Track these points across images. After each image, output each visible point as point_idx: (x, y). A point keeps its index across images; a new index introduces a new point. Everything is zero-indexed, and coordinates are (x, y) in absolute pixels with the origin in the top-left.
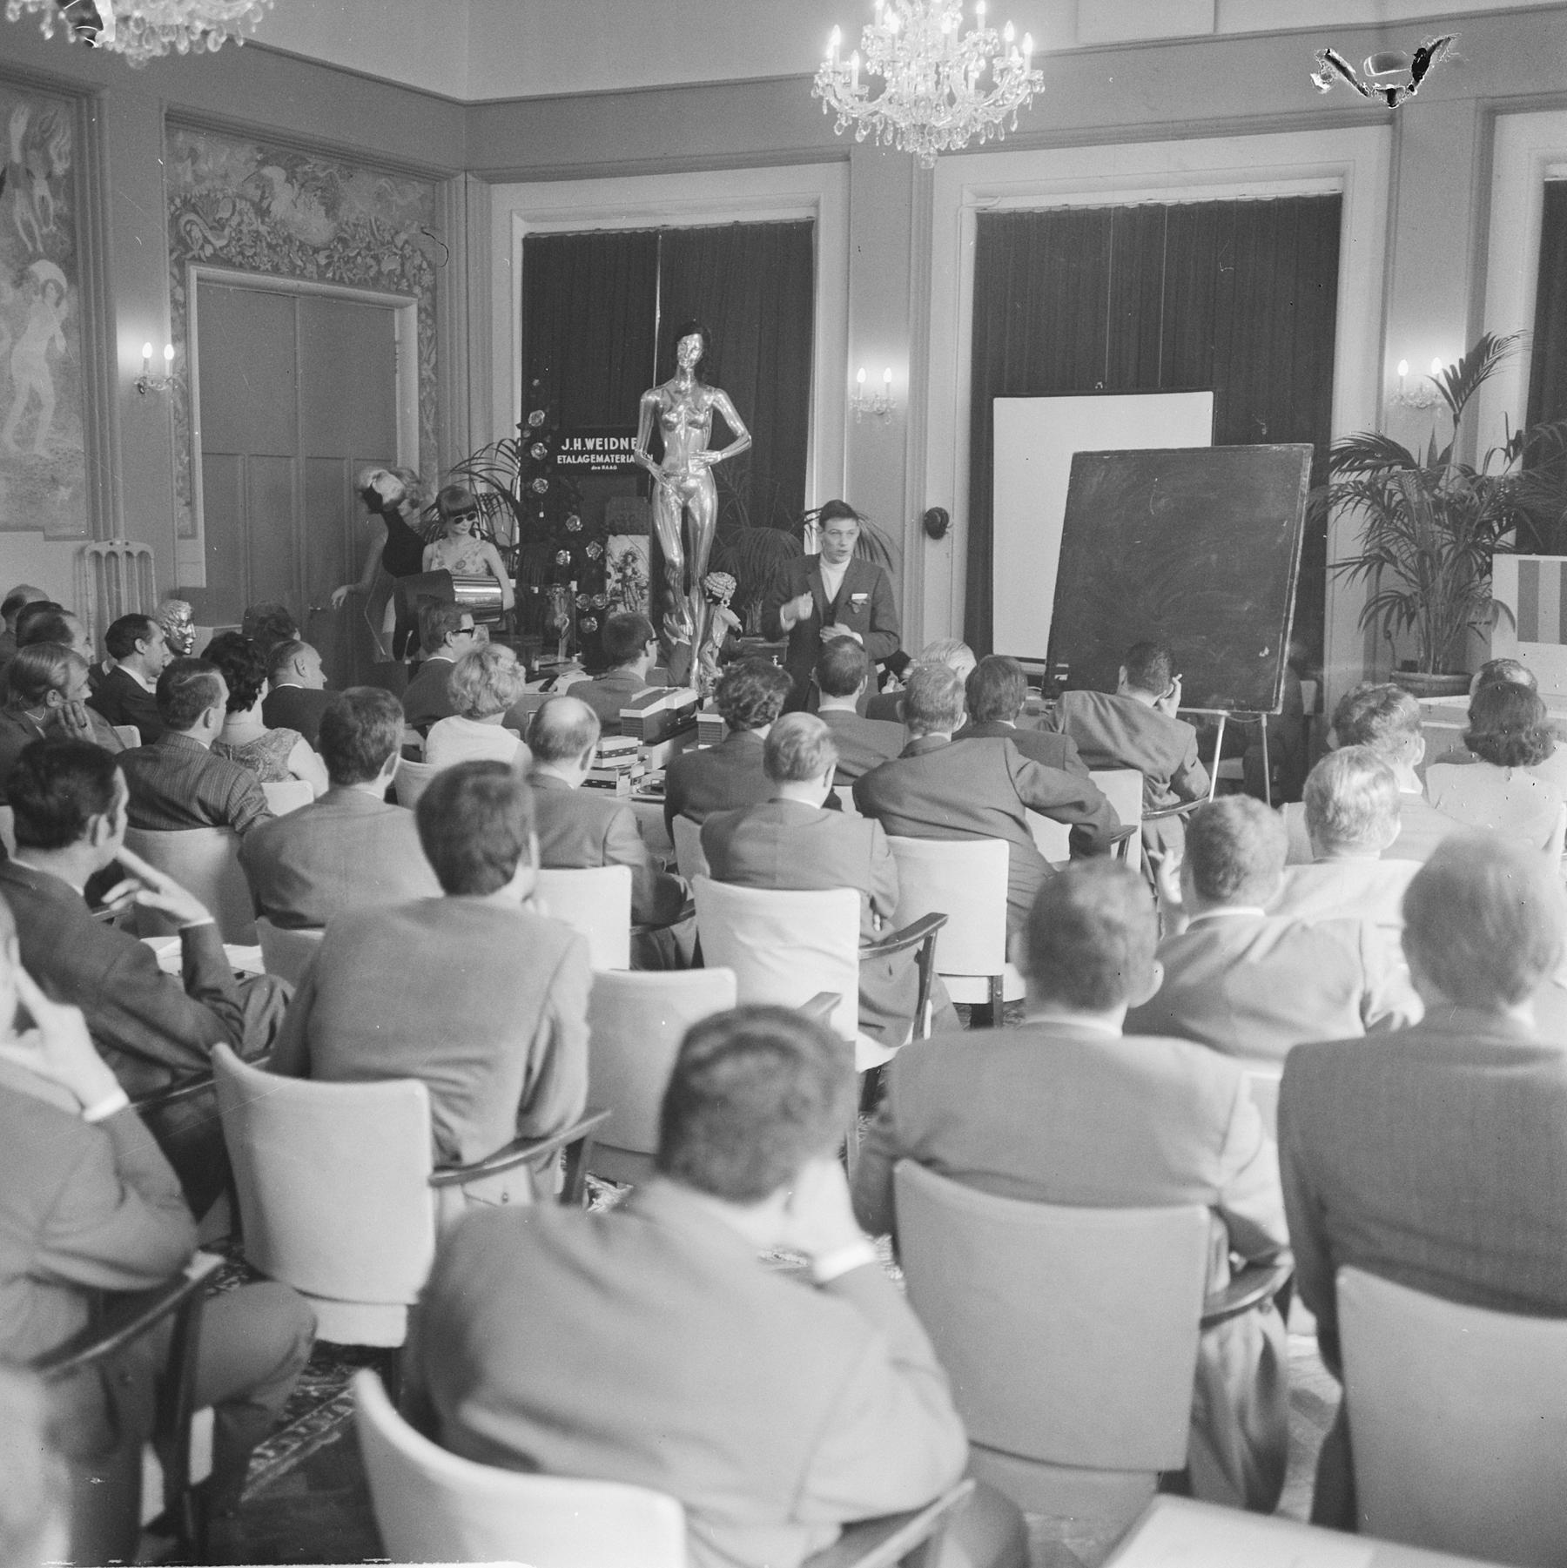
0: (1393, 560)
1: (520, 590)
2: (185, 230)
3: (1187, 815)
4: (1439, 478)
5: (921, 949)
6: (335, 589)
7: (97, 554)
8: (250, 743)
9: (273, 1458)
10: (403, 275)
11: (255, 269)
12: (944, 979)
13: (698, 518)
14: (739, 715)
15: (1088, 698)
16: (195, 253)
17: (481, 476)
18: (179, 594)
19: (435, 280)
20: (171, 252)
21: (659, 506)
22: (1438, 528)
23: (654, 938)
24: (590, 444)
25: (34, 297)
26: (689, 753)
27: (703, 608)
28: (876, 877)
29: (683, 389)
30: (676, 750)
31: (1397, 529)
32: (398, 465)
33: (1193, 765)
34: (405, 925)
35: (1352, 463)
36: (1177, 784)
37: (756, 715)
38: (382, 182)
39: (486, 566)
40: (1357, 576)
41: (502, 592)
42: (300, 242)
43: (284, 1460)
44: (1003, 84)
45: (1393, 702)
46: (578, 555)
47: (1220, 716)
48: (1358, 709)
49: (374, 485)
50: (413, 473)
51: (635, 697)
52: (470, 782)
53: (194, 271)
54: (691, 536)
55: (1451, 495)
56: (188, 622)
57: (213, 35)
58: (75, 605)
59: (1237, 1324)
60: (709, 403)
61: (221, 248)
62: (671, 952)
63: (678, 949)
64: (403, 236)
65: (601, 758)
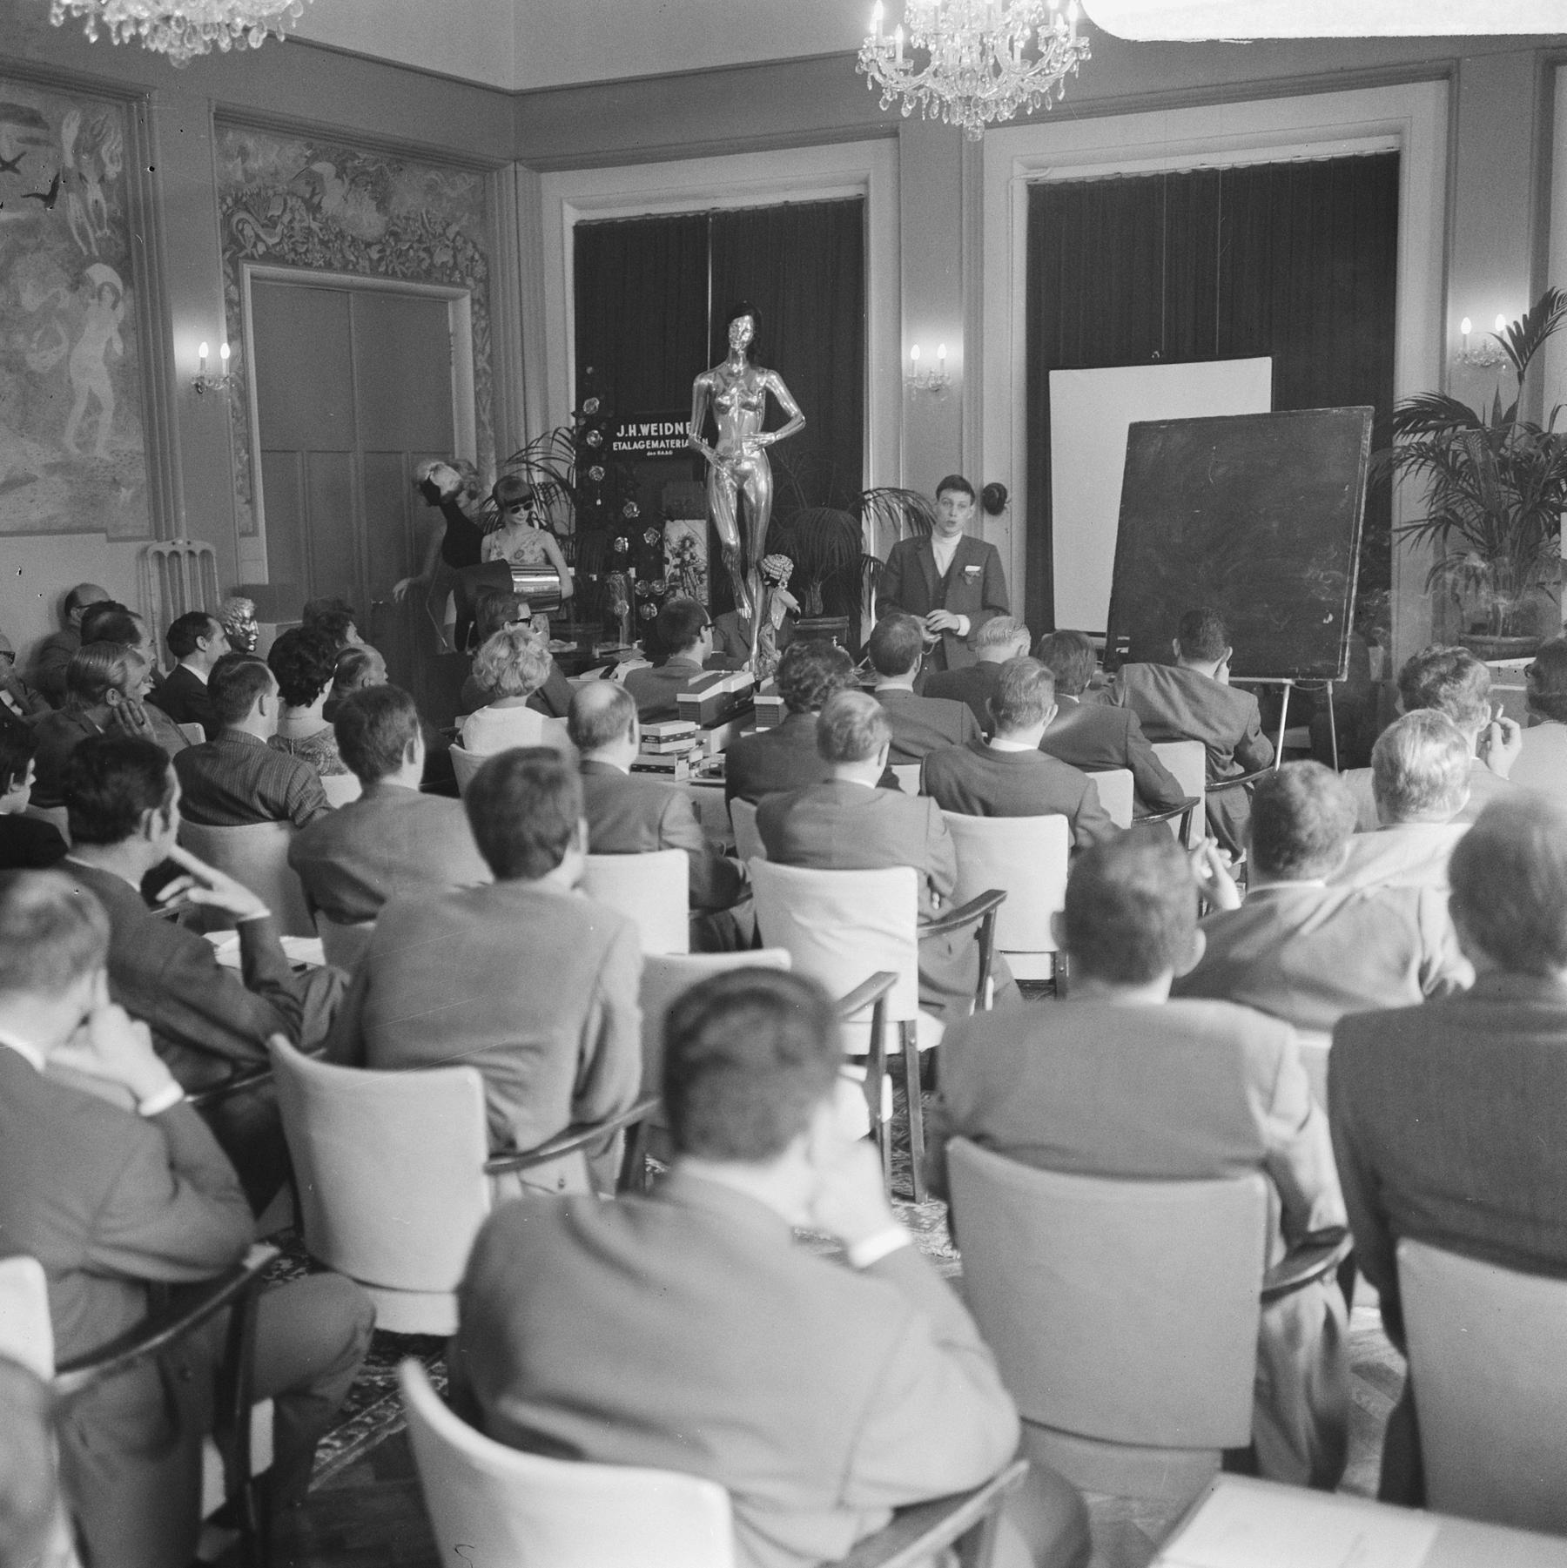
0: (1459, 522)
1: (579, 578)
2: (237, 227)
3: (1250, 785)
4: (1505, 436)
5: (981, 926)
6: (397, 581)
7: (160, 555)
8: (310, 737)
9: (340, 1448)
11: (308, 265)
12: (1007, 957)
13: (753, 499)
14: (798, 696)
15: (1148, 671)
16: (248, 250)
17: (538, 466)
18: (242, 592)
19: (488, 270)
20: (224, 251)
21: (714, 490)
22: (1505, 488)
23: (712, 921)
24: (645, 430)
25: (90, 301)
26: (747, 737)
27: (761, 591)
28: (933, 856)
29: (736, 371)
30: (734, 733)
31: (1462, 490)
32: (457, 456)
33: (1256, 734)
34: (455, 913)
36: (1240, 753)
37: (816, 698)
38: (433, 175)
39: (543, 555)
40: (1423, 539)
41: (559, 581)
42: (352, 237)
43: (352, 1450)
44: (1049, 52)
45: (1465, 670)
46: (636, 541)
47: (1282, 686)
48: (1426, 674)
49: (432, 477)
50: (470, 464)
51: (692, 681)
52: (521, 766)
53: (247, 270)
54: (748, 520)
55: (1517, 454)
56: (252, 619)
57: (254, 32)
58: (139, 608)
59: (1305, 1294)
60: (762, 384)
61: (274, 245)
62: (731, 935)
63: (738, 931)
64: (454, 228)
65: (659, 743)
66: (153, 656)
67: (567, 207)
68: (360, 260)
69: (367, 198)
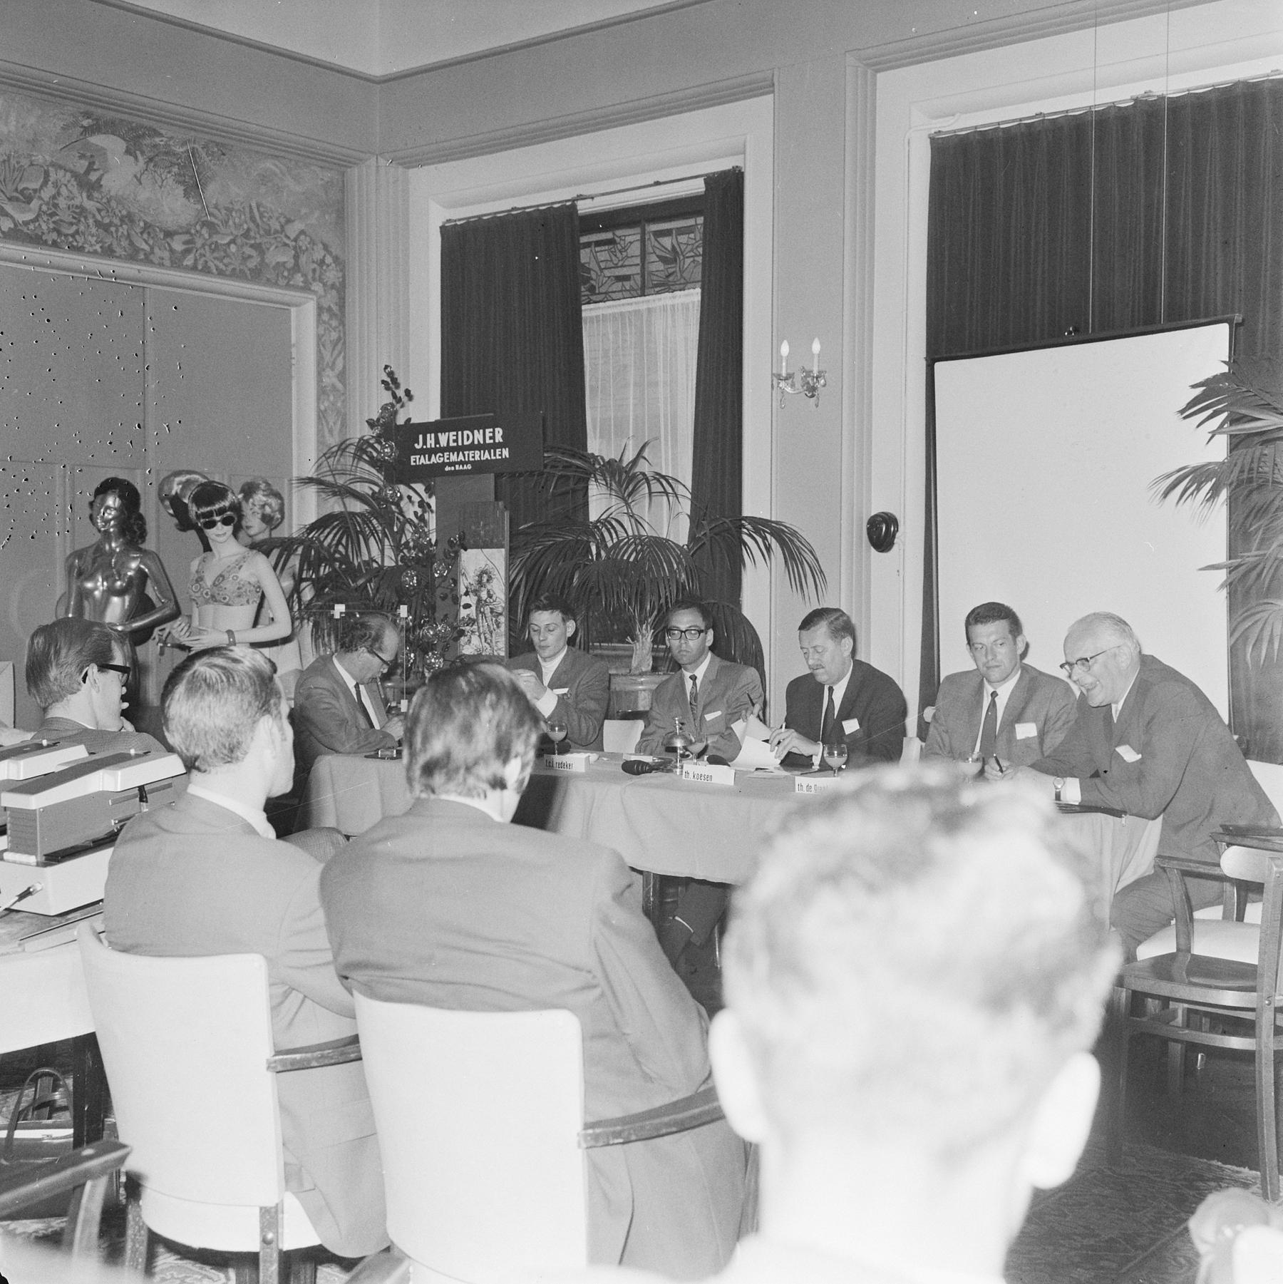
10: (296, 268)
11: (79, 250)
42: (146, 223)
68: (156, 250)
69: (170, 181)
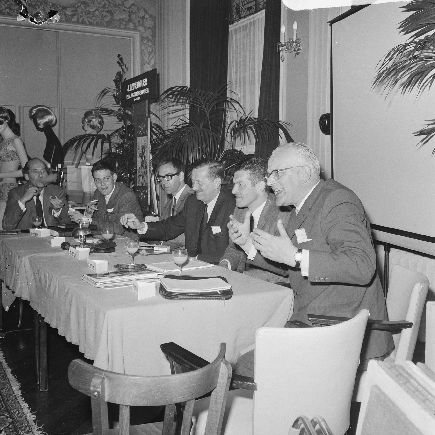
35: (156, 134)
66: (32, 193)
67: (183, 235)
